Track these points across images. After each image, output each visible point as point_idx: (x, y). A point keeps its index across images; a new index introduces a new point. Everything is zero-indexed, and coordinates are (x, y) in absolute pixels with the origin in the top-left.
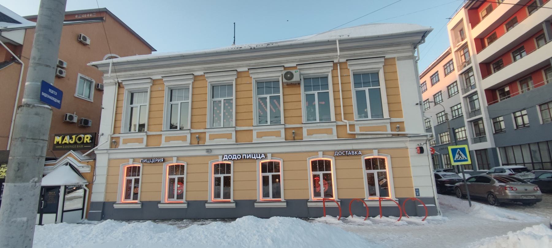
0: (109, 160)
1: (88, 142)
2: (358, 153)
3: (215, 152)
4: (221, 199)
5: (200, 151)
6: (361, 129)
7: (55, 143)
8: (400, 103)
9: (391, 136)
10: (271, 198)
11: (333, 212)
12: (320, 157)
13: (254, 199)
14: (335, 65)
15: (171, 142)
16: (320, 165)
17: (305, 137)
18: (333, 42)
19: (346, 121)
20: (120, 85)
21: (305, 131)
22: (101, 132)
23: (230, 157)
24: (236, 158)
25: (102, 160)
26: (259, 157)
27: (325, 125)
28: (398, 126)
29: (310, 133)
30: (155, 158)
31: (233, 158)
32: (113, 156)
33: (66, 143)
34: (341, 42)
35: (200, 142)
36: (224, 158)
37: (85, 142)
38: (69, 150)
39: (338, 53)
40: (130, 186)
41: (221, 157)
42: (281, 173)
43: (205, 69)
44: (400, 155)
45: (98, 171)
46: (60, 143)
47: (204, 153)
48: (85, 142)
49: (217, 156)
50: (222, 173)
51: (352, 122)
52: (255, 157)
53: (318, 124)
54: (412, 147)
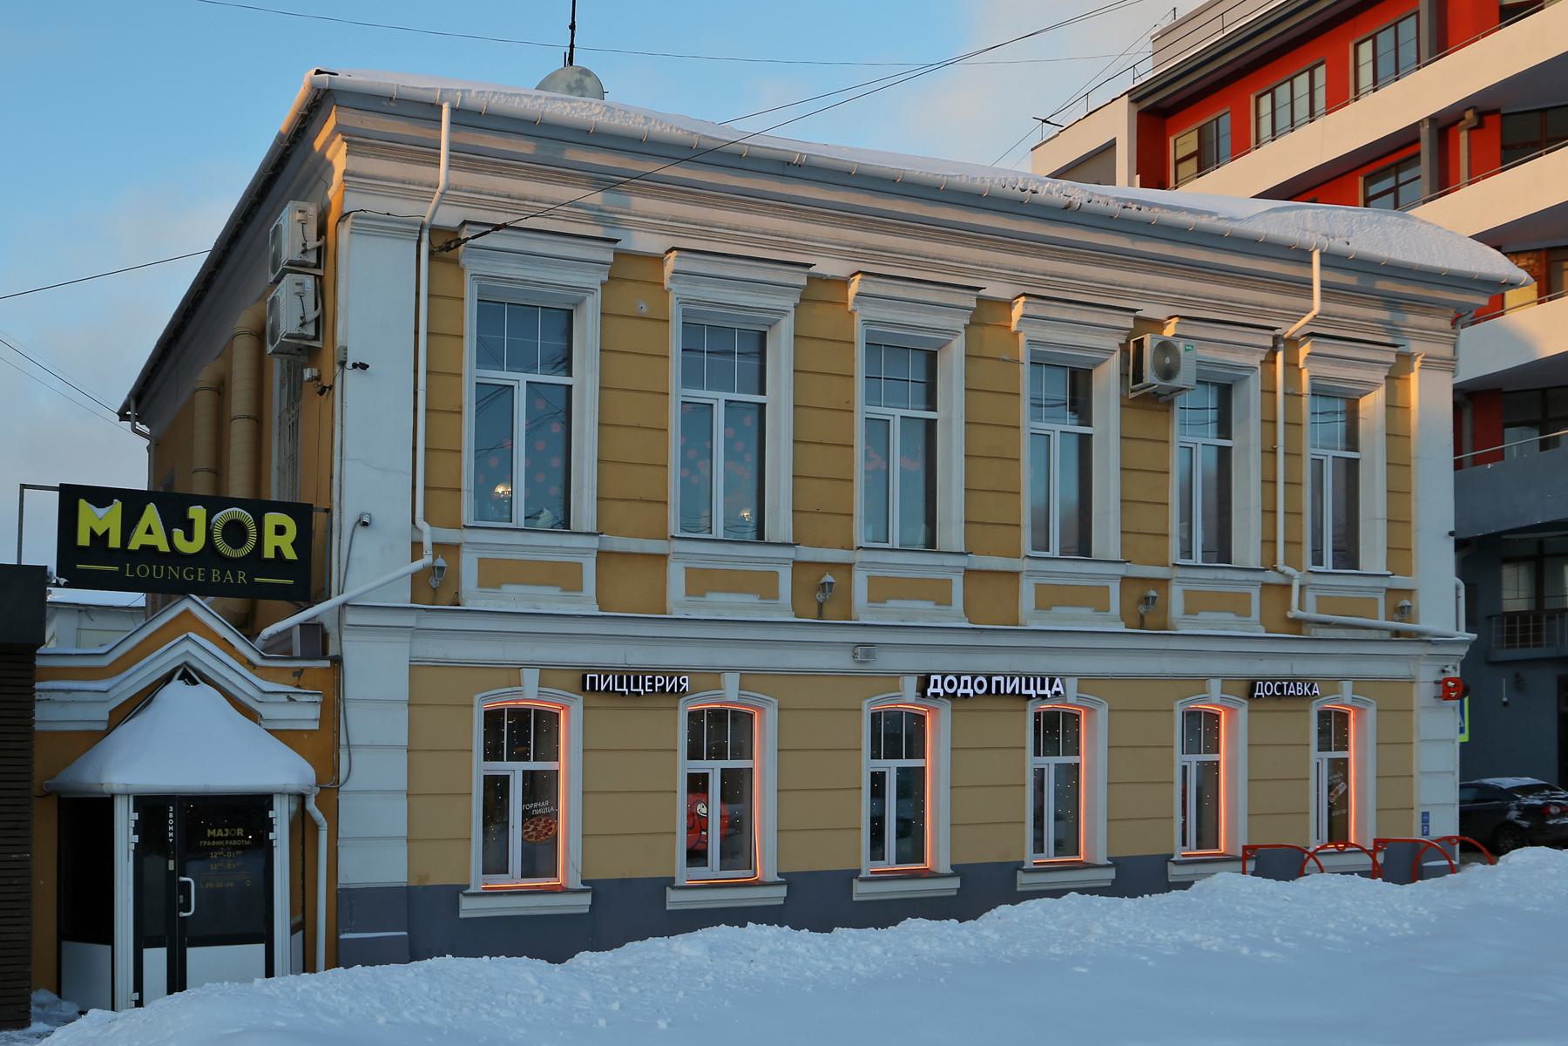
0: (415, 667)
1: (290, 554)
2: (1310, 689)
3: (888, 661)
4: (1049, 856)
5: (827, 654)
6: (1322, 604)
7: (84, 539)
8: (1409, 522)
9: (1386, 635)
10: (514, 878)
11: (935, 909)
12: (529, 693)
13: (1014, 858)
14: (1276, 339)
15: (713, 597)
16: (518, 732)
17: (473, 595)
18: (427, 110)
19: (1289, 570)
20: (445, 245)
21: (469, 566)
22: (349, 509)
23: (951, 684)
24: (969, 691)
25: (376, 669)
26: (1047, 692)
27: (548, 546)
28: (829, 578)
29: (1194, 604)
30: (654, 672)
31: (961, 691)
32: (435, 649)
33: (149, 551)
34: (465, 117)
35: (827, 609)
36: (931, 690)
37: (269, 553)
38: (183, 589)
39: (1317, 304)
40: (701, 809)
41: (911, 684)
42: (1351, 755)
43: (1183, 300)
44: (1393, 700)
45: (360, 724)
46: (115, 542)
47: (841, 661)
48: (269, 553)
49: (895, 677)
50: (893, 753)
51: (449, 536)
52: (1032, 692)
53: (517, 538)
54: (1427, 674)
